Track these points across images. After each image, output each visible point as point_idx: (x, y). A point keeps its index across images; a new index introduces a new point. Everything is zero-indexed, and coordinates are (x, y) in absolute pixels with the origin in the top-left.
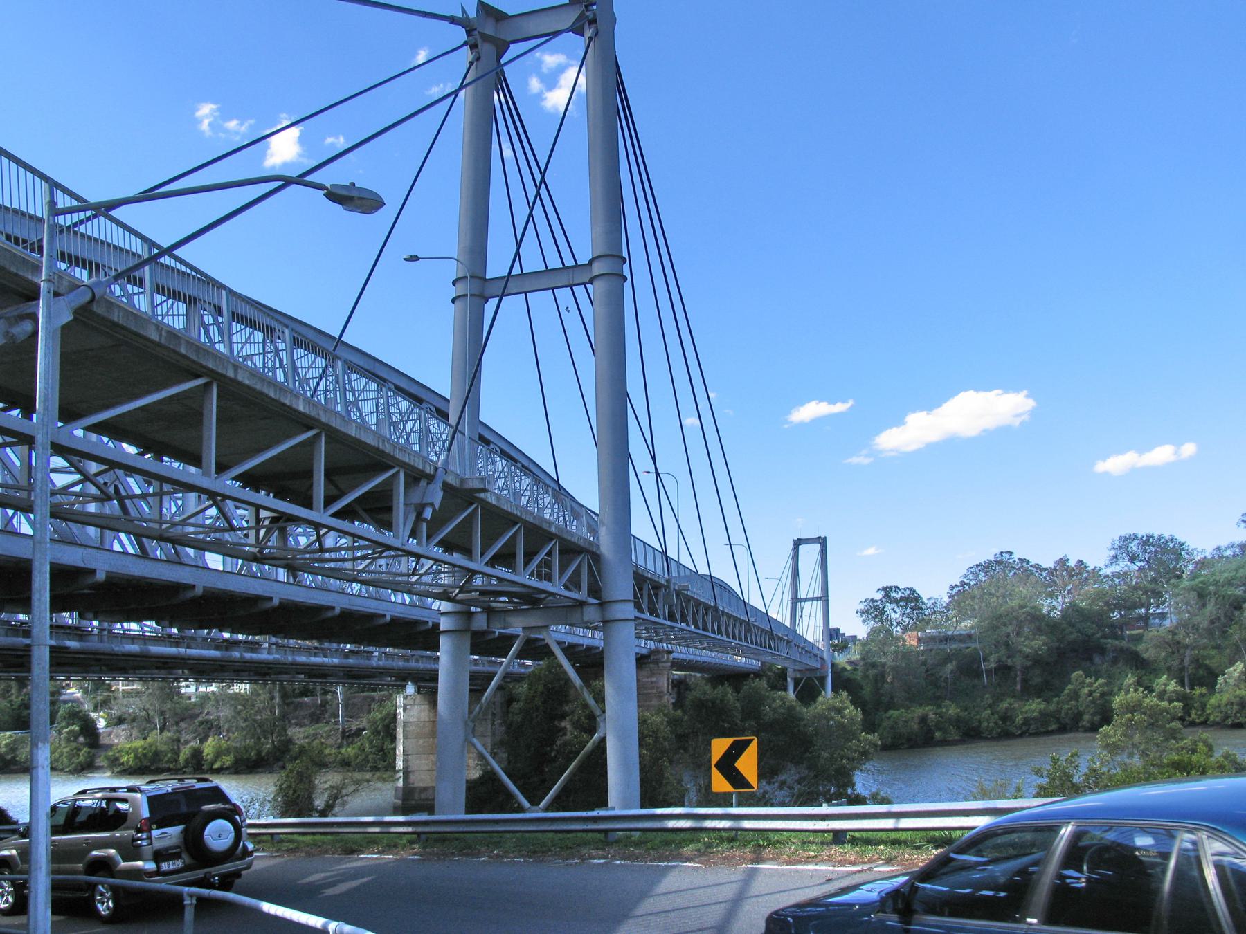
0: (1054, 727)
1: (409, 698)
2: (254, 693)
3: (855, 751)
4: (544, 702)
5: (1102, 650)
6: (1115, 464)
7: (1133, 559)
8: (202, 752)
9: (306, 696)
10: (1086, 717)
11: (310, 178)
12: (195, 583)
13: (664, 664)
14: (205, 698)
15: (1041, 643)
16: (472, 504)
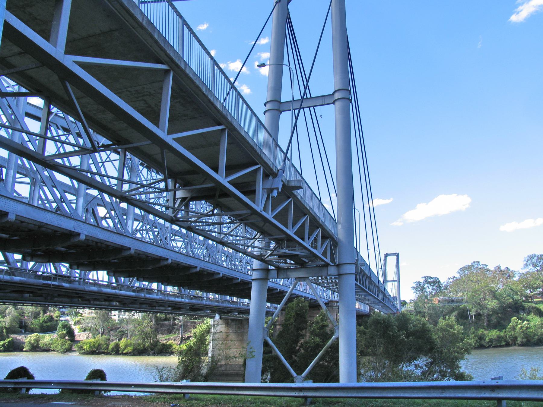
0: (504, 343)
1: (216, 321)
2: (144, 319)
3: (462, 349)
4: (295, 321)
5: (524, 309)
6: (509, 227)
7: (534, 266)
8: (119, 345)
9: (166, 321)
10: (519, 339)
12: (131, 247)
13: (335, 308)
14: (122, 321)
15: (496, 303)
16: (289, 198)
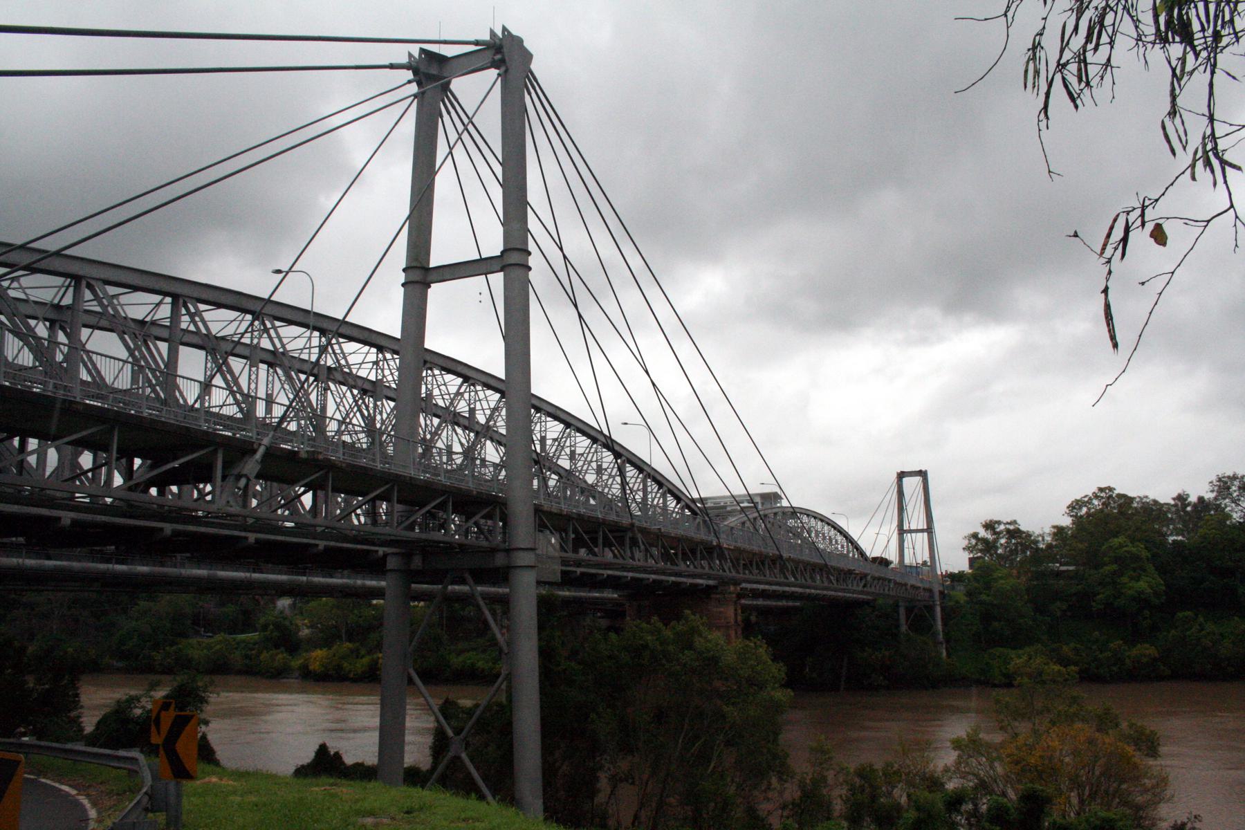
11: (450, 156)
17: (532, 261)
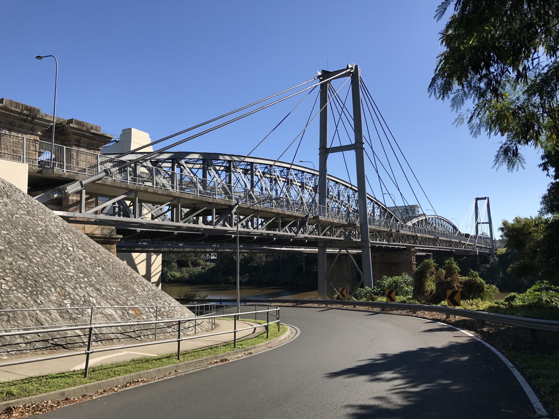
17: (364, 146)
